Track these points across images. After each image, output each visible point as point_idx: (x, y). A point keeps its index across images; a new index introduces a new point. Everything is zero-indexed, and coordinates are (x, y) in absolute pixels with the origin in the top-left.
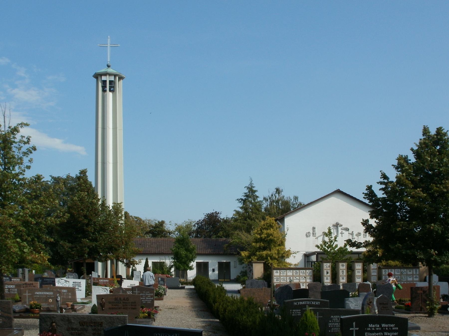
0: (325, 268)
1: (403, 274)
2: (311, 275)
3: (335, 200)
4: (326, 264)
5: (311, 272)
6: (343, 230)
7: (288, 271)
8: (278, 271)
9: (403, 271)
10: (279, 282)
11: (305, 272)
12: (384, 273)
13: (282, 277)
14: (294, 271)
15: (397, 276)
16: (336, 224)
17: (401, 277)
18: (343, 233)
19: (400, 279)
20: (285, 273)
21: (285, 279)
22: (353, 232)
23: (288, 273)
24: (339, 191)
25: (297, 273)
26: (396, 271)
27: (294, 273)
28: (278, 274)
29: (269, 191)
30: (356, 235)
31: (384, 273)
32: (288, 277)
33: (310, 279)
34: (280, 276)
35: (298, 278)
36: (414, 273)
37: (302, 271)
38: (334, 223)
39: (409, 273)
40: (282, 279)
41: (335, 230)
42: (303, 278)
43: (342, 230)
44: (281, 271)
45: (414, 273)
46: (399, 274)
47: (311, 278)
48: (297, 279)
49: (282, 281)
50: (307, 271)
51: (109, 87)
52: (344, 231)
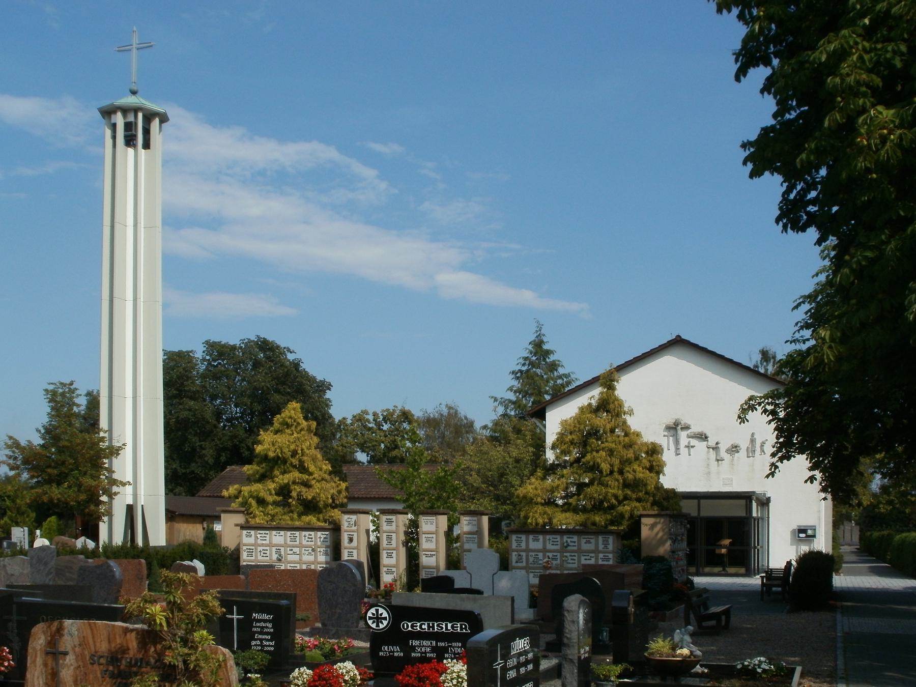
0: (346, 528)
1: (569, 548)
2: (328, 544)
3: (669, 363)
4: (348, 516)
5: (328, 536)
6: (692, 437)
7: (274, 532)
8: (253, 532)
9: (569, 540)
10: (253, 558)
11: (313, 536)
12: (603, 546)
13: (260, 548)
14: (289, 533)
15: (550, 555)
16: (674, 424)
17: (562, 556)
18: (693, 447)
19: (559, 562)
20: (267, 538)
21: (268, 552)
22: (717, 443)
23: (274, 537)
24: (679, 339)
25: (294, 539)
26: (548, 541)
27: (289, 539)
28: (251, 540)
29: (750, 358)
30: (727, 451)
31: (603, 546)
32: (274, 549)
33: (326, 554)
34: (256, 545)
35: (296, 550)
36: (601, 547)
37: (307, 533)
38: (670, 422)
39: (585, 547)
40: (260, 552)
41: (671, 438)
42: (310, 551)
43: (690, 439)
44: (258, 532)
45: (601, 547)
46: (558, 547)
47: (329, 552)
48: (295, 553)
49: (260, 558)
50: (319, 534)
51: (126, 137)
52: (694, 442)
